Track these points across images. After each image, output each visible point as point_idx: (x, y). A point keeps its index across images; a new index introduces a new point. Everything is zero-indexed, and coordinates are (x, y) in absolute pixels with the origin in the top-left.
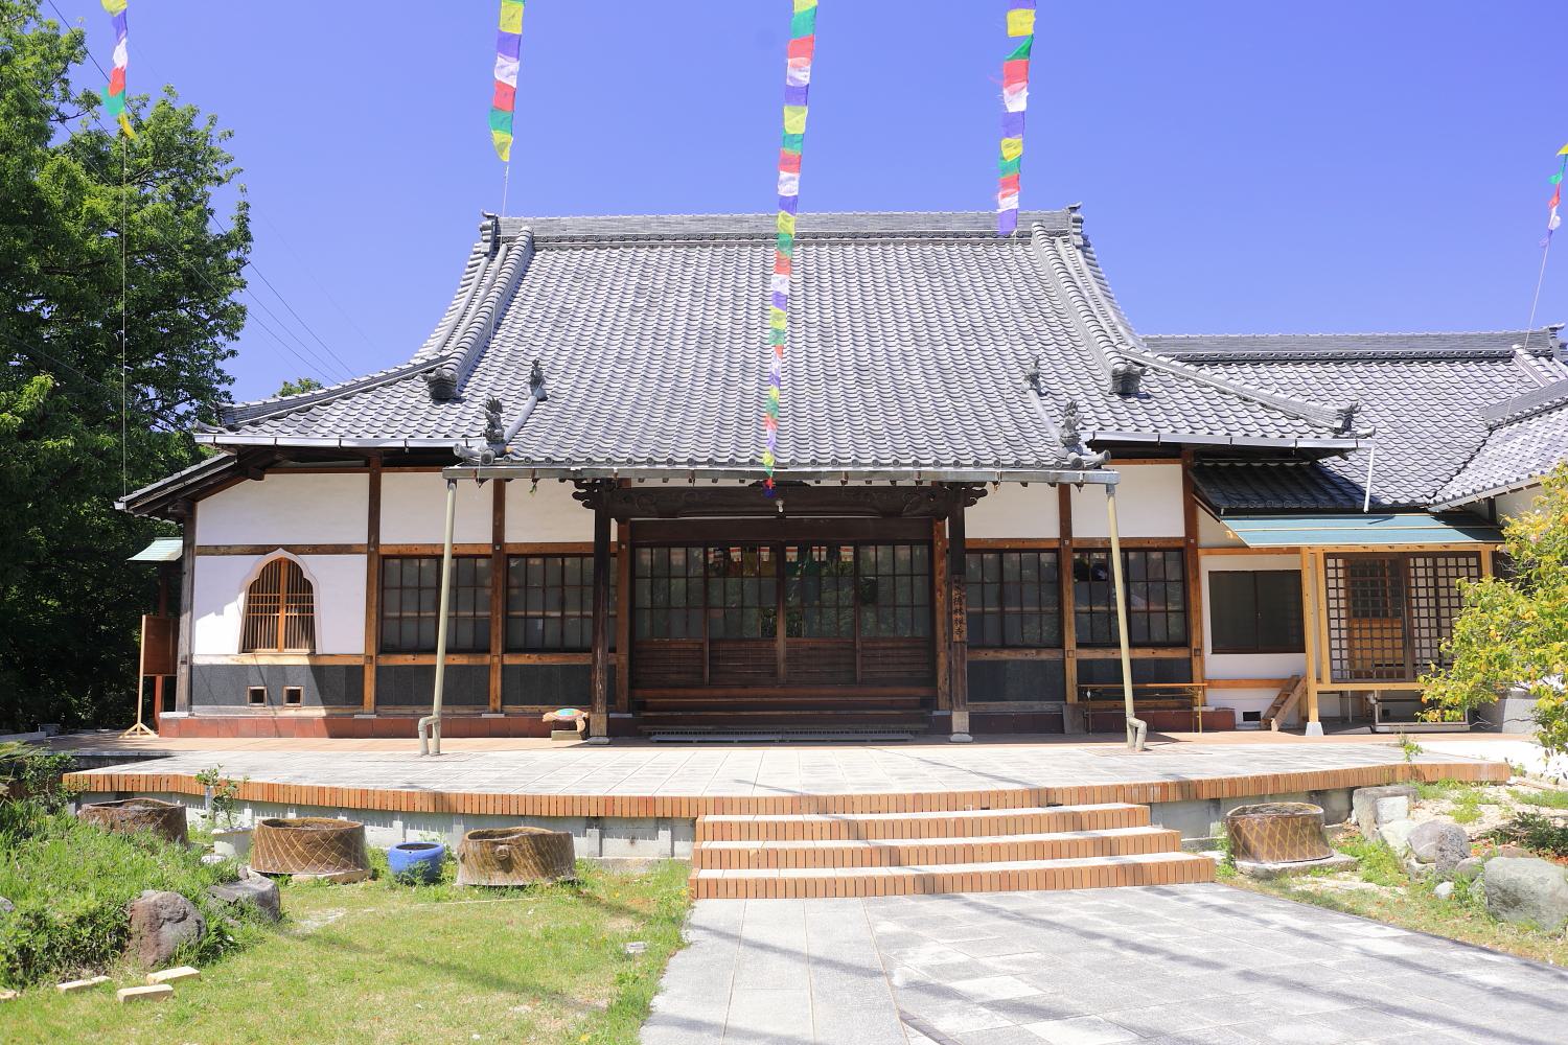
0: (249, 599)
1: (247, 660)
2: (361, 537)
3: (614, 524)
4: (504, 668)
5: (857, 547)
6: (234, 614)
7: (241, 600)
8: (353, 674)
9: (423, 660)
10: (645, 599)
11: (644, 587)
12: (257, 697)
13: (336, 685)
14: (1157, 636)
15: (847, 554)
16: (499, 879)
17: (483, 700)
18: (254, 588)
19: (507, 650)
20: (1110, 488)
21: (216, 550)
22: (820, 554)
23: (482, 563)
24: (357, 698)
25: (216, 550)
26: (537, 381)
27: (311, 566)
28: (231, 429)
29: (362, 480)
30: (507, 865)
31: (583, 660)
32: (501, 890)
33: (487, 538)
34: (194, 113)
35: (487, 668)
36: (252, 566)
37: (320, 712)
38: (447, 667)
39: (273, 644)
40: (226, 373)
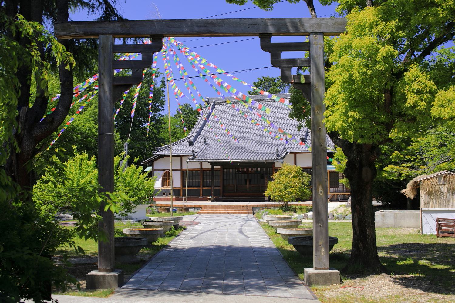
0: (163, 178)
1: (163, 188)
2: (180, 168)
3: (219, 167)
4: (214, 190)
6: (160, 181)
7: (161, 178)
8: (179, 190)
9: (190, 188)
10: (225, 178)
11: (225, 176)
12: (164, 194)
13: (176, 192)
14: (194, 185)
17: (199, 195)
19: (203, 186)
20: (282, 163)
23: (199, 172)
24: (180, 195)
26: (205, 142)
28: (158, 152)
31: (210, 188)
35: (200, 190)
36: (162, 173)
37: (174, 197)
38: (188, 190)
39: (166, 186)
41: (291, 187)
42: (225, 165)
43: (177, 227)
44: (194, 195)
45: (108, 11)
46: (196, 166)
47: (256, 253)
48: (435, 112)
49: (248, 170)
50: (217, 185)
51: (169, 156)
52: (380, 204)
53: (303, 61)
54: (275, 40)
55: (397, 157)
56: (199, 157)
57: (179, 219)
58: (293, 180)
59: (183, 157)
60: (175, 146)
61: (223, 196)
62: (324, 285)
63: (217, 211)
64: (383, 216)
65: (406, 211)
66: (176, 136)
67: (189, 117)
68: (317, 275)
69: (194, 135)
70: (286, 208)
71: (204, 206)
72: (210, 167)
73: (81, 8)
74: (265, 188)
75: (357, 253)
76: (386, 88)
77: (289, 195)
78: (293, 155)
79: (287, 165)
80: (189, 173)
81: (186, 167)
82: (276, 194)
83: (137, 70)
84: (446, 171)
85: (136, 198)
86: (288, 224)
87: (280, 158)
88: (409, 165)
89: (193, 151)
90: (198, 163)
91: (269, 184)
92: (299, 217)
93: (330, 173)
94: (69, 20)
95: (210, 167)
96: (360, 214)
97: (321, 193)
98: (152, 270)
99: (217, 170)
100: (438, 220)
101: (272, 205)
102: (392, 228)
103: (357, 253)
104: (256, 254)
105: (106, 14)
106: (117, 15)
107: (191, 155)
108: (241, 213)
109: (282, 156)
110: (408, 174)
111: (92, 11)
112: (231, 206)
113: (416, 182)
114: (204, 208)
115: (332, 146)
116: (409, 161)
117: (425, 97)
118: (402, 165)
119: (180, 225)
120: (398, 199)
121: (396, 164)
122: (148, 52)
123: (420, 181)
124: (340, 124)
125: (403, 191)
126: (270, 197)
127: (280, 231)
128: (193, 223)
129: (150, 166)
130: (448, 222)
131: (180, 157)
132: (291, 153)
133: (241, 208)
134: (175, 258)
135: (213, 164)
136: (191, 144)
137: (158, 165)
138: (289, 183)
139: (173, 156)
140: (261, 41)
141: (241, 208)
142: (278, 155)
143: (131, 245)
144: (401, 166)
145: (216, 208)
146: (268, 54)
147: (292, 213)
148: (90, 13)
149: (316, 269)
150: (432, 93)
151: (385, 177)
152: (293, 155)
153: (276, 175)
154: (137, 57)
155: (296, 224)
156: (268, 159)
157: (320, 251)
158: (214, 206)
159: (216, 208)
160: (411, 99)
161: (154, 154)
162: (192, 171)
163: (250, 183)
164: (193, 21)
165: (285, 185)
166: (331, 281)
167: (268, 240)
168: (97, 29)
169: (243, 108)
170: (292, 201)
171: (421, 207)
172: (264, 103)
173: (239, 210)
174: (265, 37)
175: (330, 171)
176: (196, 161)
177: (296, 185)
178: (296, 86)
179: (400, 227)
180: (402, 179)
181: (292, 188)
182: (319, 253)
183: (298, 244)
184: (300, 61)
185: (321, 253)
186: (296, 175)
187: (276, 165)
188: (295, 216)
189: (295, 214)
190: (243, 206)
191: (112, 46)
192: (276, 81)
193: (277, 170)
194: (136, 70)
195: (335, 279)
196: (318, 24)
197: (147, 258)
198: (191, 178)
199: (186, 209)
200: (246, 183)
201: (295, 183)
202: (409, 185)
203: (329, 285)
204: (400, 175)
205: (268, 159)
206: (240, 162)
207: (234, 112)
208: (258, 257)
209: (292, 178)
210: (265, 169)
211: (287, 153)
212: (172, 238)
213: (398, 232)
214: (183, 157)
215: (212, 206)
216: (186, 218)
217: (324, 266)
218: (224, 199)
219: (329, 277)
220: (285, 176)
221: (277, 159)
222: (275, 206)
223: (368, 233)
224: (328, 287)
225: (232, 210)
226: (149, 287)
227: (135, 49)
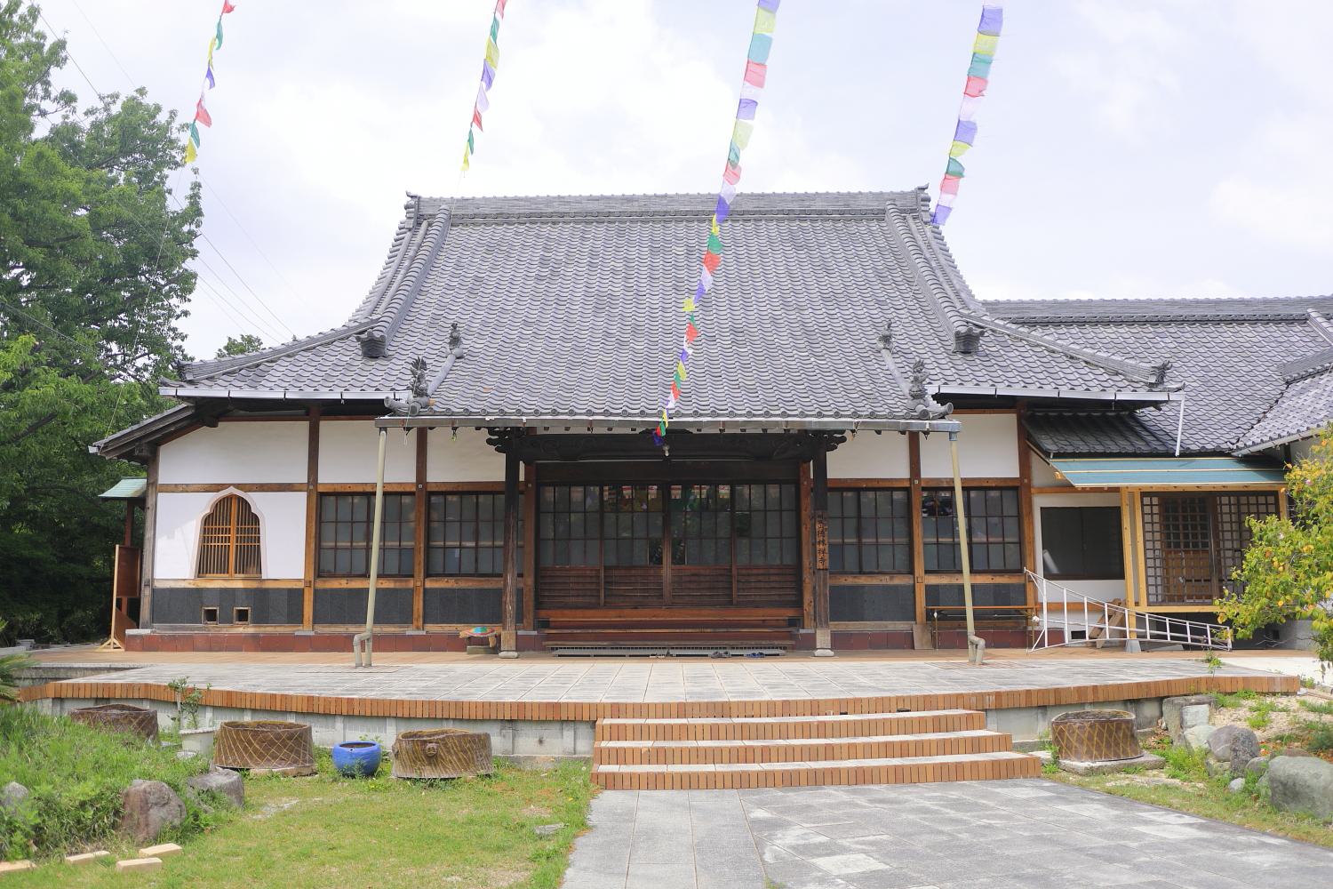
11: (548, 520)
16: (429, 773)
18: (208, 520)
23: (406, 500)
26: (455, 341)
27: (258, 502)
30: (433, 759)
33: (413, 480)
34: (158, 109)
35: (412, 592)
40: (179, 331)
131: (304, 426)
137: (177, 464)
163: (678, 560)
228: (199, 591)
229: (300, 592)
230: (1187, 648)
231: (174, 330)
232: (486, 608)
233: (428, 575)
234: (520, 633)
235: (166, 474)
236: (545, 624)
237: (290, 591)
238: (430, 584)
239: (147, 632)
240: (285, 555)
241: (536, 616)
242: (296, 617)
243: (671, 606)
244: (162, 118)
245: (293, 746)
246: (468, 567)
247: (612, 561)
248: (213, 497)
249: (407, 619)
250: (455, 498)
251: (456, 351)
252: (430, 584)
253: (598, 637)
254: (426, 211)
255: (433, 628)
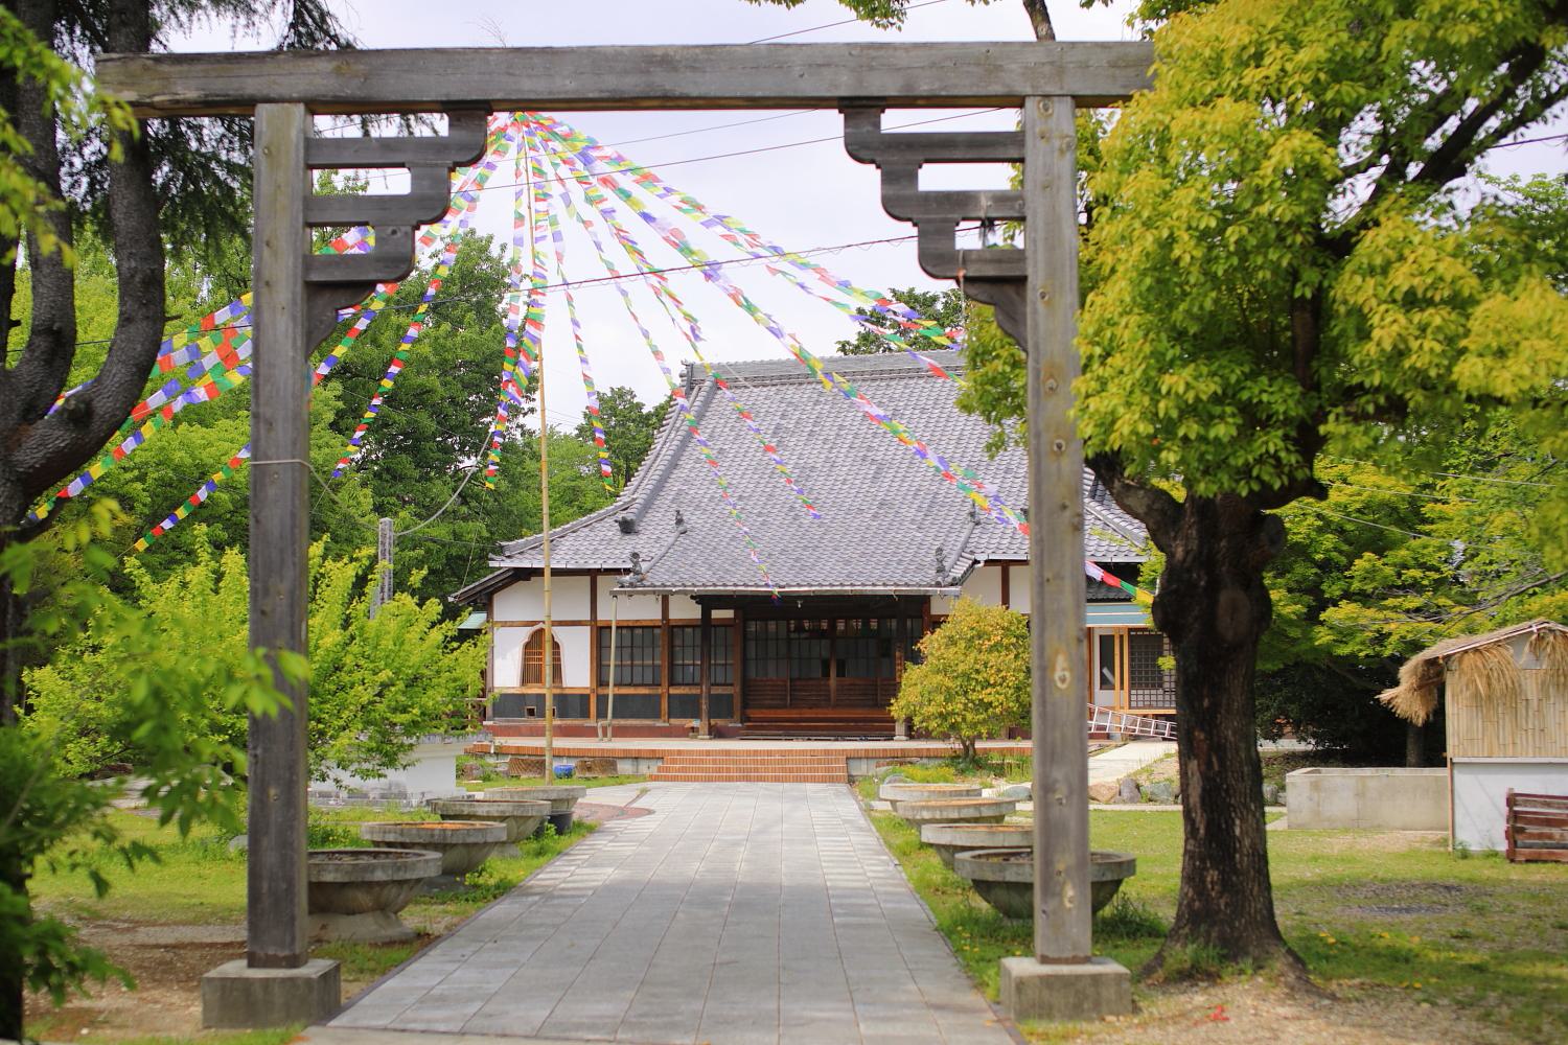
3: (729, 614)
4: (711, 697)
5: (880, 619)
11: (752, 645)
15: (874, 624)
16: (588, 775)
18: (527, 646)
21: (505, 624)
22: (857, 624)
23: (657, 631)
25: (505, 624)
26: (679, 522)
27: (561, 634)
29: (588, 578)
30: (589, 769)
31: (695, 691)
32: (588, 779)
33: (659, 616)
34: (490, 239)
35: (659, 697)
36: (524, 634)
40: (527, 427)
41: (987, 684)
42: (753, 607)
43: (561, 822)
44: (634, 711)
45: (305, 24)
46: (647, 611)
47: (839, 911)
48: (1469, 373)
49: (833, 626)
50: (720, 679)
51: (539, 572)
52: (1310, 747)
53: (1000, 198)
54: (895, 121)
55: (1371, 574)
56: (659, 577)
57: (570, 800)
58: (993, 659)
59: (600, 579)
60: (570, 538)
61: (745, 719)
62: (1071, 1018)
63: (719, 770)
64: (1316, 786)
65: (1398, 772)
66: (574, 502)
67: (624, 431)
68: (1047, 981)
69: (641, 497)
70: (970, 761)
71: (670, 752)
72: (694, 612)
73: (213, 14)
74: (893, 689)
75: (1197, 904)
76: (1297, 294)
77: (978, 712)
78: (998, 569)
79: (968, 610)
80: (620, 637)
81: (613, 611)
82: (932, 709)
83: (394, 232)
84: (1542, 619)
85: (416, 711)
86: (966, 813)
87: (949, 580)
88: (1414, 601)
89: (635, 555)
90: (653, 597)
91: (905, 675)
92: (1015, 791)
93: (1130, 636)
94: (154, 47)
95: (694, 612)
96: (1209, 764)
97: (1063, 680)
98: (450, 967)
99: (724, 623)
100: (1512, 800)
101: (920, 754)
102: (1347, 830)
103: (1197, 904)
104: (839, 915)
105: (299, 34)
106: (335, 38)
107: (627, 571)
108: (805, 780)
109: (958, 572)
110: (1410, 637)
111: (247, 26)
112: (769, 753)
113: (1431, 662)
114: (674, 761)
115: (1137, 537)
116: (1415, 587)
117: (1437, 321)
118: (1390, 602)
119: (575, 818)
120: (1374, 730)
121: (1364, 598)
122: (437, 170)
123: (1448, 658)
124: (1130, 426)
125: (1386, 695)
126: (909, 720)
127: (929, 834)
128: (624, 812)
129: (477, 609)
130: (1549, 805)
131: (588, 578)
132: (989, 562)
133: (805, 762)
134: (541, 925)
135: (708, 601)
136: (627, 527)
137: (509, 606)
138: (978, 672)
139: (556, 572)
140: (846, 126)
141: (805, 762)
142: (940, 570)
143: (379, 876)
144: (1386, 608)
145: (714, 762)
146: (870, 177)
147: (991, 779)
148: (241, 31)
149: (1045, 960)
150: (1461, 304)
151: (1327, 650)
152: (998, 569)
153: (930, 643)
154: (396, 182)
155: (995, 816)
156: (907, 585)
157: (1060, 895)
158: (708, 753)
159: (714, 762)
160: (1388, 327)
161: (492, 564)
162: (632, 628)
163: (841, 673)
164: (599, 53)
165: (966, 676)
166: (1097, 1006)
167: (891, 868)
168: (249, 80)
169: (817, 403)
170: (991, 737)
171: (1449, 753)
172: (893, 383)
173: (799, 770)
174: (859, 108)
175: (1130, 630)
176: (644, 593)
177: (1004, 678)
178: (972, 291)
179: (1379, 828)
180: (1387, 653)
181: (989, 690)
182: (1052, 904)
183: (990, 876)
184: (987, 199)
185: (1061, 903)
186: (1005, 641)
187: (936, 610)
188: (993, 790)
189: (1002, 781)
190: (813, 753)
191: (302, 145)
192: (939, 306)
193: (937, 623)
194: (390, 230)
195: (1113, 997)
196: (1052, 63)
197: (442, 925)
198: (627, 652)
199: (603, 766)
200: (827, 675)
201: (999, 671)
202: (1405, 672)
203: (1090, 1020)
204: (1381, 638)
205: (907, 585)
206: (808, 599)
207: (783, 416)
208: (845, 926)
209: (990, 650)
210: (894, 623)
211: (976, 562)
212: (542, 860)
213: (1366, 843)
214: (600, 579)
215: (700, 752)
216: (596, 798)
217: (1074, 949)
218: (748, 728)
219: (1090, 991)
220: (962, 644)
221: (938, 584)
222: (931, 756)
223: (1237, 831)
224: (1085, 1026)
225: (774, 770)
226: (429, 1021)
227: (386, 155)
228: (523, 696)
229: (588, 696)
230: (1164, 739)
231: (521, 426)
232: (686, 707)
233: (672, 684)
234: (713, 722)
235: (498, 615)
236: (749, 719)
237: (582, 695)
238: (673, 691)
239: (490, 723)
240: (577, 674)
241: (743, 714)
242: (585, 714)
243: (836, 706)
244: (495, 251)
245: (539, 766)
246: (649, 679)
247: (796, 675)
248: (530, 630)
249: (657, 715)
250: (690, 630)
251: (681, 528)
252: (673, 691)
253: (778, 728)
254: (698, 377)
255: (675, 722)
